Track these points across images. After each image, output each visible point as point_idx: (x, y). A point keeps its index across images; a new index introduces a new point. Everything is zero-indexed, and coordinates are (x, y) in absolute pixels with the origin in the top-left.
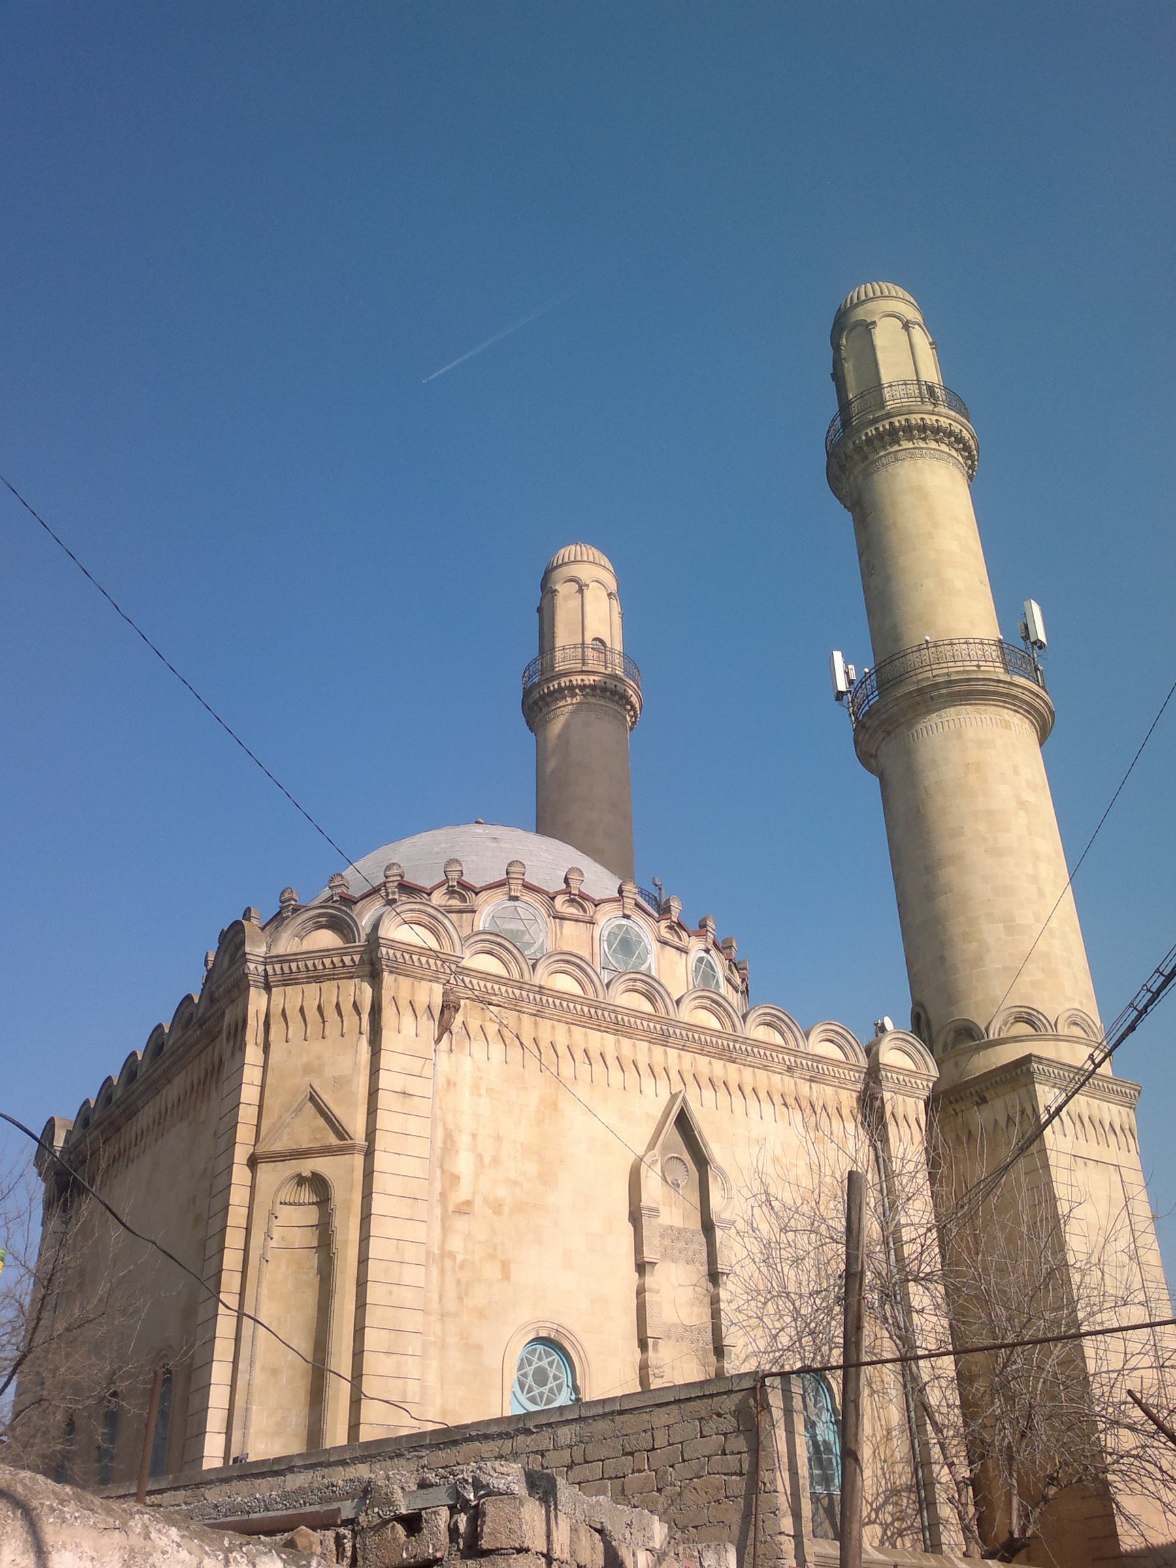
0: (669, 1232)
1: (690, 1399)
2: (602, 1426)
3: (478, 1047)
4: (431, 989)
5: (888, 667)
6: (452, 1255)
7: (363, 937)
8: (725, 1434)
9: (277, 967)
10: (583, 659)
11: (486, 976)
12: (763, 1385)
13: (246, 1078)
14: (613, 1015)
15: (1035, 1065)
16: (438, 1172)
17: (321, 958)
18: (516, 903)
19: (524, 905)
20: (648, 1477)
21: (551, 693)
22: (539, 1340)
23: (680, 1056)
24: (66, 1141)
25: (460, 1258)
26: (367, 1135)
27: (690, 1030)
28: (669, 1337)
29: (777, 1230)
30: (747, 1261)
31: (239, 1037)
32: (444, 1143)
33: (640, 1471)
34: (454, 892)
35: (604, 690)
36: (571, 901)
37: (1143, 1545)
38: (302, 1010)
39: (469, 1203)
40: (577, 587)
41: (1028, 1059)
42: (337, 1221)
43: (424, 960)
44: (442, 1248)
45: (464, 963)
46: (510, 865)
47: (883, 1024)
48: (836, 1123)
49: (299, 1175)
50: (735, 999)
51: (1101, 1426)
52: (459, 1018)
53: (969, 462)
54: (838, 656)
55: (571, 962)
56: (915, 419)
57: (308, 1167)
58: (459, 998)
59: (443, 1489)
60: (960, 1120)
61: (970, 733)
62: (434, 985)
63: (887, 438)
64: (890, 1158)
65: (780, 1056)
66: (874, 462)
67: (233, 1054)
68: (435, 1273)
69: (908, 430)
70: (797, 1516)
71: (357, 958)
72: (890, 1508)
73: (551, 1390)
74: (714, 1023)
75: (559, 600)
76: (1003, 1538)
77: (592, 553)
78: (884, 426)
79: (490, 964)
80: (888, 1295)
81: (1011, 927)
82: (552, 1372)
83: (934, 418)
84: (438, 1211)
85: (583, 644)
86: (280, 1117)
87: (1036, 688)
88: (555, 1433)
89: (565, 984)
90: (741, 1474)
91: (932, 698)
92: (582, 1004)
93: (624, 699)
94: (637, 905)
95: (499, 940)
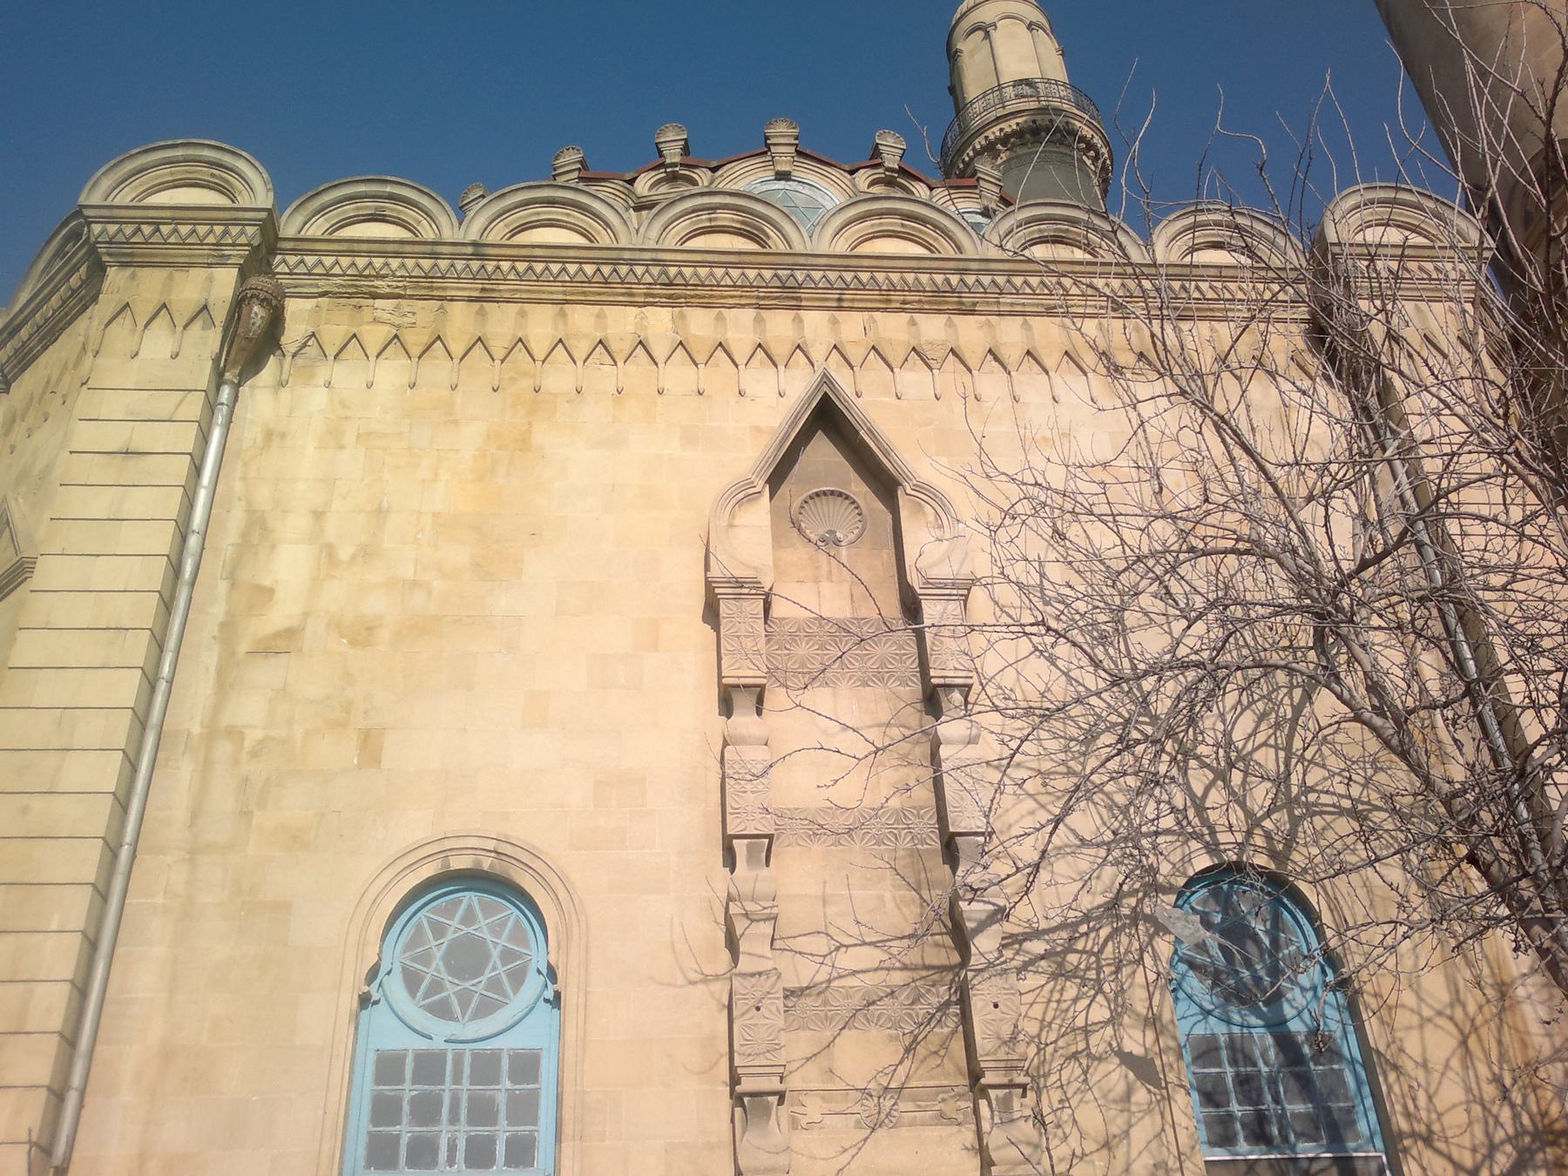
6: (235, 734)
25: (253, 736)
27: (847, 268)
32: (245, 534)
39: (291, 633)
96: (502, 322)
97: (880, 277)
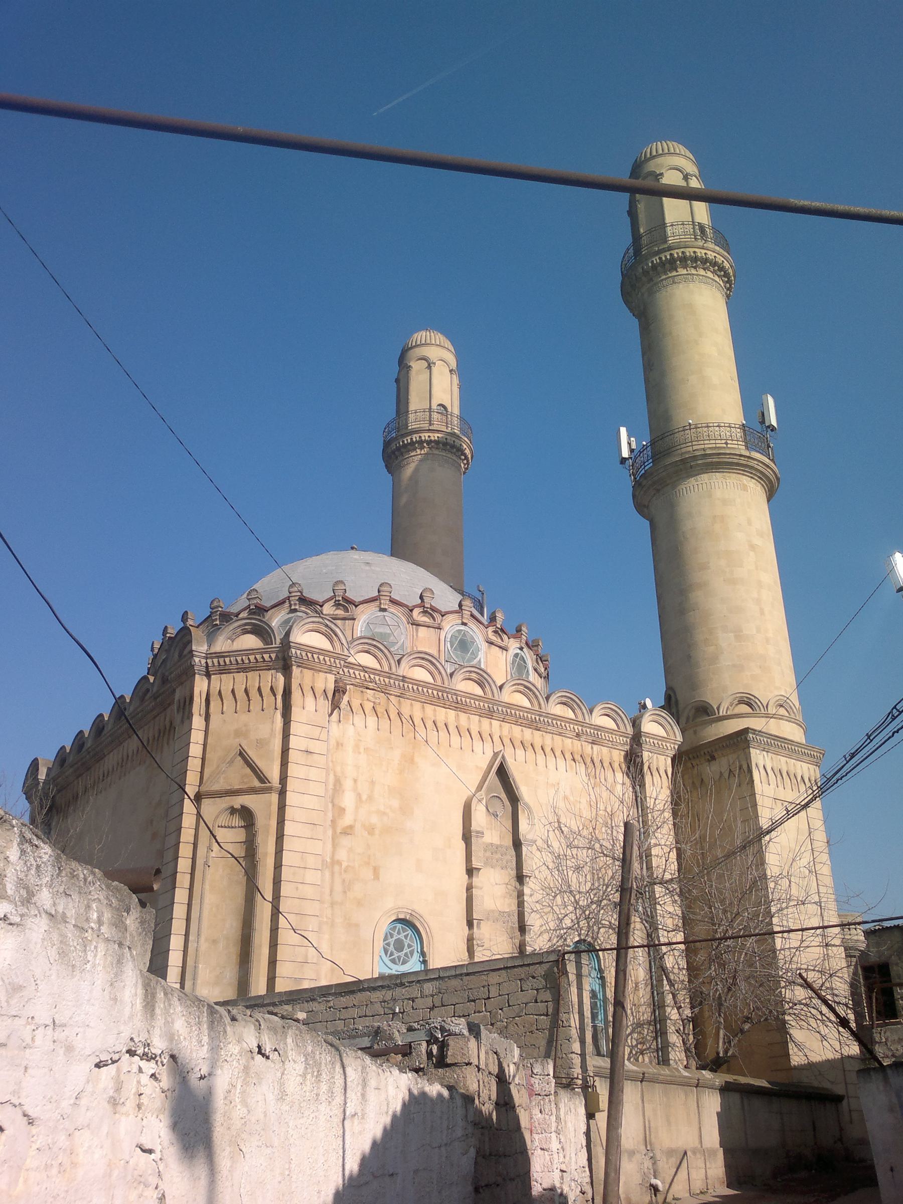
0: (493, 849)
1: (514, 967)
2: (455, 983)
3: (358, 719)
4: (326, 678)
5: (660, 442)
6: (339, 863)
7: (278, 641)
8: (537, 990)
9: (215, 661)
10: (430, 421)
11: (364, 669)
12: (564, 959)
13: (193, 738)
14: (454, 697)
15: (751, 735)
16: (330, 805)
17: (247, 655)
18: (385, 614)
19: (391, 615)
20: (485, 1016)
21: (405, 446)
22: (399, 920)
23: (501, 726)
24: (47, 775)
26: (281, 780)
27: (509, 708)
28: (488, 919)
29: (565, 847)
30: (544, 867)
31: (187, 710)
32: (335, 785)
33: (479, 1012)
34: (340, 604)
35: (445, 444)
36: (425, 612)
37: (806, 1062)
38: (233, 691)
39: (351, 827)
40: (426, 364)
41: (746, 731)
42: (259, 839)
43: (321, 657)
44: (332, 858)
45: (351, 660)
46: (381, 585)
47: (645, 703)
48: (609, 774)
49: (232, 807)
50: (539, 682)
51: (783, 984)
52: (346, 698)
53: (728, 285)
54: (623, 431)
55: (426, 659)
56: (689, 252)
57: (238, 801)
58: (346, 684)
59: (423, 1032)
60: (695, 771)
61: (718, 494)
62: (328, 675)
63: (667, 266)
64: (645, 798)
65: (572, 726)
66: (657, 283)
67: (182, 722)
68: (327, 874)
69: (684, 259)
70: (583, 1042)
71: (273, 656)
72: (635, 1035)
73: (406, 955)
74: (526, 703)
75: (413, 373)
76: (712, 1056)
77: (439, 338)
78: (666, 256)
79: (367, 660)
80: (641, 894)
81: (739, 635)
82: (406, 942)
83: (704, 251)
84: (330, 833)
85: (430, 408)
86: (218, 767)
87: (768, 460)
88: (422, 987)
89: (421, 674)
90: (547, 1015)
91: (691, 467)
92: (433, 689)
93: (461, 451)
94: (472, 615)
95: (375, 643)
96: (406, 707)
97: (517, 713)
